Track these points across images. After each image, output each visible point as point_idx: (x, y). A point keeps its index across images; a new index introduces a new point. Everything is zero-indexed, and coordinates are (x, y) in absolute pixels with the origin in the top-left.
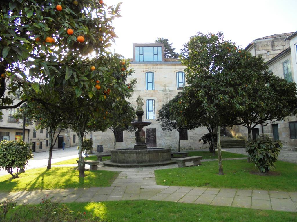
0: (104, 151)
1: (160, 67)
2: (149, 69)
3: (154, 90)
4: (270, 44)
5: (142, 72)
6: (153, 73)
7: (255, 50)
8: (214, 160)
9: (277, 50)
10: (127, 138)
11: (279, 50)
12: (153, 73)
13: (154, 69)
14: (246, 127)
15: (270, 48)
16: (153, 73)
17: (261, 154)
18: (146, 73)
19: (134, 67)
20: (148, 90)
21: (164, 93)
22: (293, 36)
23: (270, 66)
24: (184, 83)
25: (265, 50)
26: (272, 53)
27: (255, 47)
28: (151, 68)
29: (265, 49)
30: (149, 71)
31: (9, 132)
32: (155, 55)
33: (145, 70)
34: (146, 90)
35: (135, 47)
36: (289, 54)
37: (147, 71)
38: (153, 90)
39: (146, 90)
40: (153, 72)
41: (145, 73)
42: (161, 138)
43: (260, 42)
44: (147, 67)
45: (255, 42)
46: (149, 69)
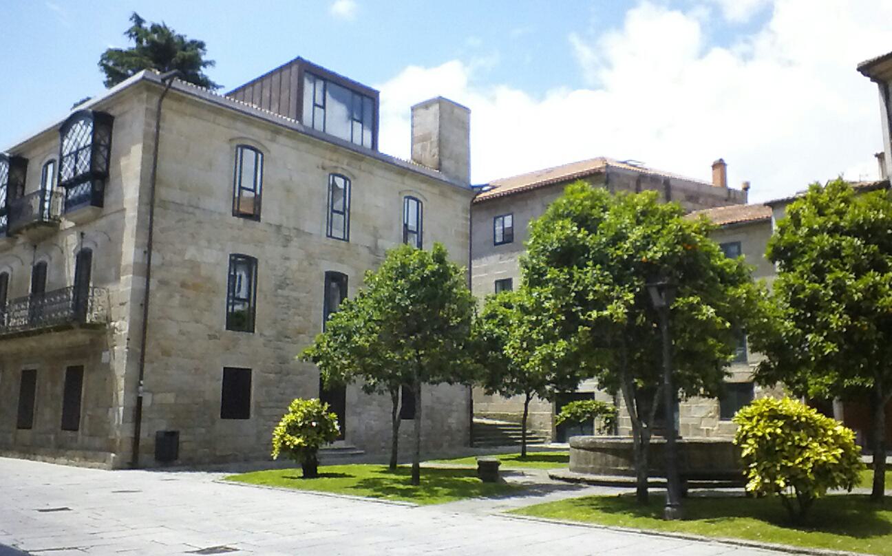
0: (181, 455)
3: (348, 240)
5: (321, 170)
8: (82, 400)
10: (262, 405)
12: (260, 156)
16: (262, 154)
17: (213, 389)
18: (330, 175)
20: (331, 236)
21: (372, 256)
24: (258, 192)
28: (344, 165)
33: (327, 163)
34: (328, 236)
35: (306, 71)
38: (344, 240)
39: (328, 236)
40: (349, 177)
41: (328, 174)
42: (358, 410)
44: (335, 157)
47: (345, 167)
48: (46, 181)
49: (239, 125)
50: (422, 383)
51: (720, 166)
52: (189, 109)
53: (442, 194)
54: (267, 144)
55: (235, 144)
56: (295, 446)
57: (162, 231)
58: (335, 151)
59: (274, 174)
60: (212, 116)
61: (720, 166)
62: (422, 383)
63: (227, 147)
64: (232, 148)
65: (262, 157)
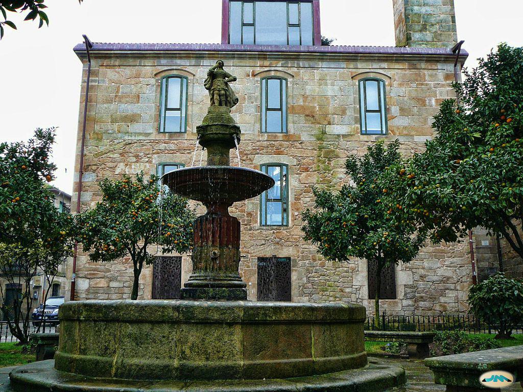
2: (273, 69)
16: (186, 78)
44: (267, 63)
46: (273, 69)
49: (163, 61)
54: (190, 69)
58: (265, 58)
60: (138, 62)
64: (157, 81)
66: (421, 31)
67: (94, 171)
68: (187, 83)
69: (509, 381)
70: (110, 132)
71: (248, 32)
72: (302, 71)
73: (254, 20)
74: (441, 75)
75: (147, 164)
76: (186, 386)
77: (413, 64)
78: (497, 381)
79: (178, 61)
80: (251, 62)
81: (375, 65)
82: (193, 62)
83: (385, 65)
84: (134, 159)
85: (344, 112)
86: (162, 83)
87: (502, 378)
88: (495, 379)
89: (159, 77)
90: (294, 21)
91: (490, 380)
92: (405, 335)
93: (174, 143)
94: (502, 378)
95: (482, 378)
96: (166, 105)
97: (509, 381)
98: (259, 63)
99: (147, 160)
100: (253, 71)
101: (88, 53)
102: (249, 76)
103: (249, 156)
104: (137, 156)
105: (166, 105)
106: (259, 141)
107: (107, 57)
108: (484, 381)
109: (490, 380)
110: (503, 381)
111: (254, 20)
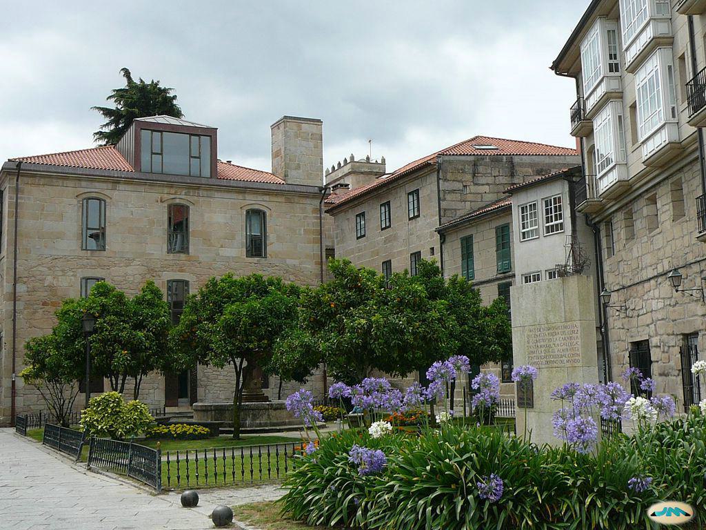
1: (205, 193)
2: (178, 196)
4: (469, 169)
5: (160, 204)
6: (103, 202)
7: (439, 179)
9: (483, 185)
11: (488, 184)
12: (103, 202)
13: (189, 198)
14: (326, 391)
15: (469, 177)
16: (105, 201)
19: (270, 205)
22: (585, 20)
23: (469, 227)
25: (459, 181)
26: (472, 191)
27: (438, 172)
29: (459, 179)
30: (94, 195)
31: (470, 237)
32: (153, 156)
36: (507, 215)
37: (84, 196)
39: (82, 250)
43: (450, 162)
44: (173, 191)
45: (440, 160)
46: (178, 196)
47: (183, 197)
48: (600, 250)
49: (84, 184)
50: (200, 367)
51: (127, 73)
52: (42, 181)
53: (289, 201)
54: (108, 192)
55: (80, 198)
56: (177, 434)
57: (318, 269)
58: (172, 187)
59: (113, 213)
60: (60, 182)
61: (127, 73)
62: (200, 367)
63: (75, 201)
64: (79, 201)
65: (105, 204)
66: (296, 169)
67: (25, 283)
68: (105, 204)
69: (687, 515)
70: (38, 247)
71: (157, 158)
72: (201, 199)
73: (162, 150)
74: (309, 208)
75: (72, 278)
76: (220, 528)
77: (289, 198)
78: (670, 516)
79: (97, 184)
80: (160, 189)
81: (260, 198)
82: (110, 186)
83: (267, 198)
84: (61, 273)
85: (233, 238)
86: (83, 204)
87: (677, 512)
88: (668, 512)
89: (80, 199)
90: (195, 153)
91: (662, 513)
92: (283, 425)
93: (94, 260)
94: (677, 512)
95: (650, 511)
96: (87, 225)
97: (687, 515)
98: (166, 190)
99: (72, 274)
100: (161, 198)
101: (19, 172)
102: (157, 201)
103: (158, 273)
104: (63, 271)
105: (87, 225)
106: (166, 260)
107: (34, 176)
108: (654, 515)
109: (662, 513)
110: (679, 516)
111: (162, 150)
